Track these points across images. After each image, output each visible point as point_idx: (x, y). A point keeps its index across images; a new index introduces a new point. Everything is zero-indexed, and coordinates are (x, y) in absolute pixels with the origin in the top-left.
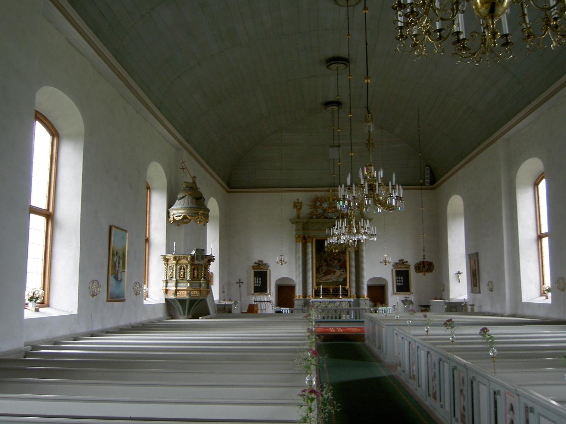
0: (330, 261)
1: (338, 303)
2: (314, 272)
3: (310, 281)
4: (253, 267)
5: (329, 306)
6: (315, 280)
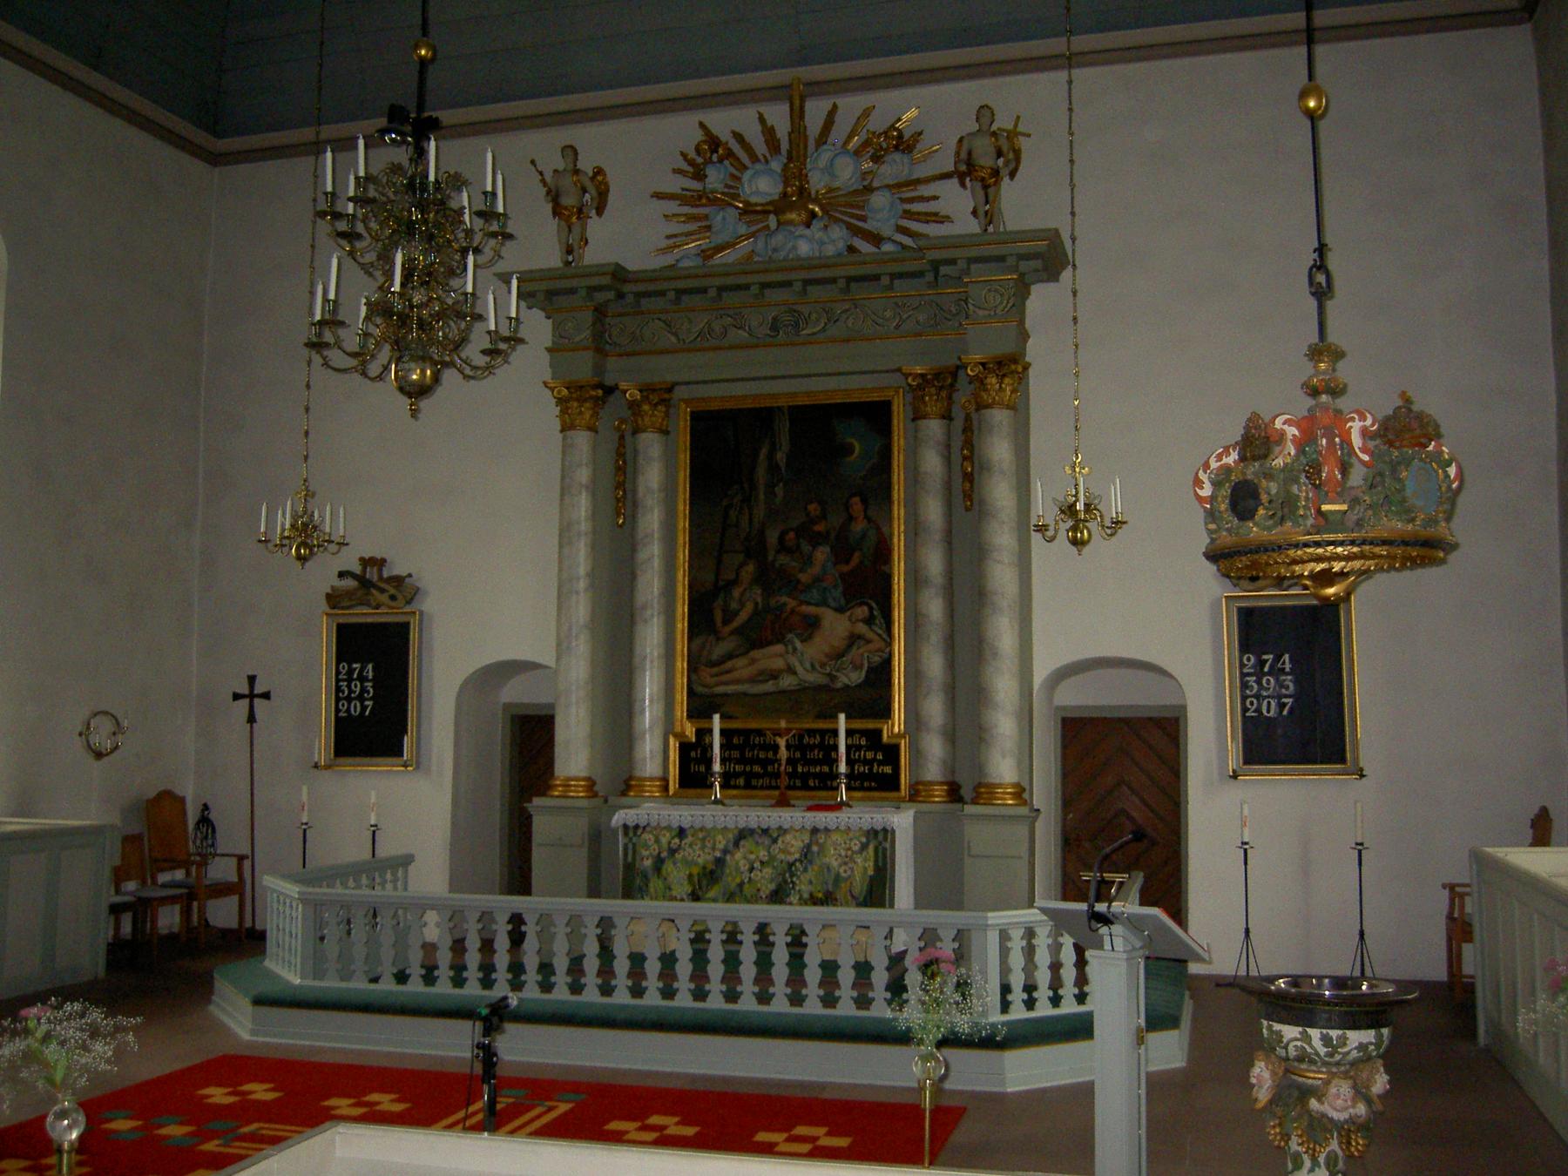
0: (783, 547)
1: (795, 844)
2: (682, 626)
3: (649, 686)
4: (334, 599)
5: (739, 859)
6: (681, 681)
